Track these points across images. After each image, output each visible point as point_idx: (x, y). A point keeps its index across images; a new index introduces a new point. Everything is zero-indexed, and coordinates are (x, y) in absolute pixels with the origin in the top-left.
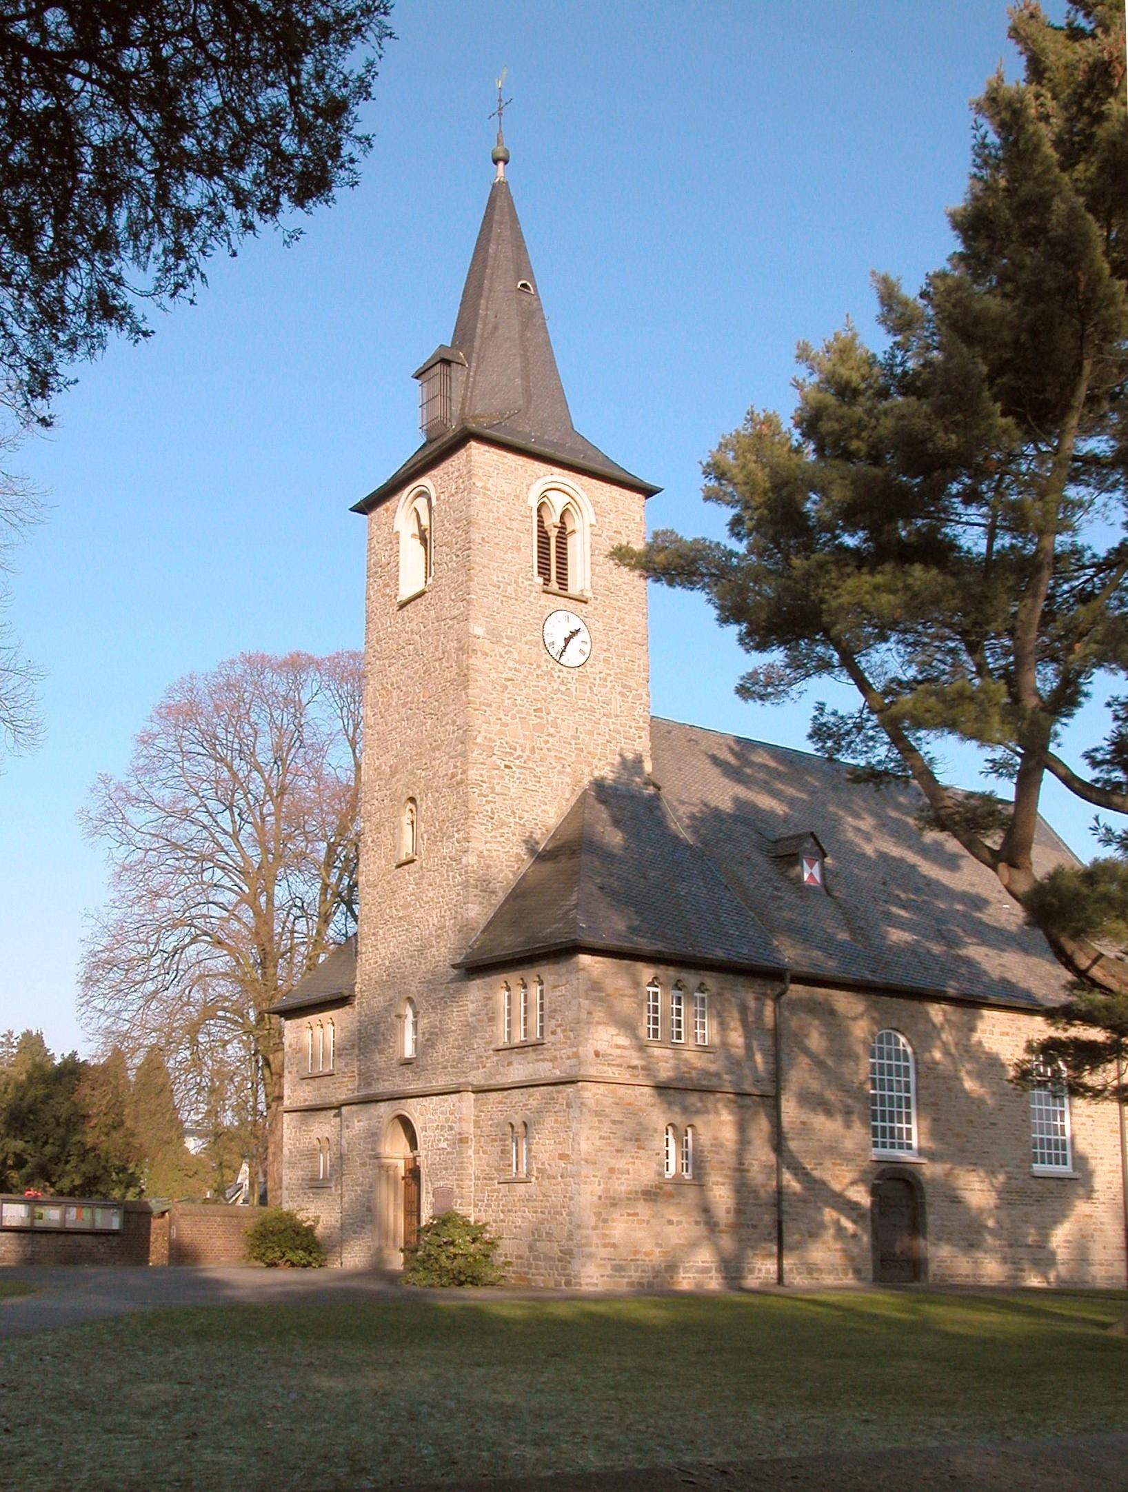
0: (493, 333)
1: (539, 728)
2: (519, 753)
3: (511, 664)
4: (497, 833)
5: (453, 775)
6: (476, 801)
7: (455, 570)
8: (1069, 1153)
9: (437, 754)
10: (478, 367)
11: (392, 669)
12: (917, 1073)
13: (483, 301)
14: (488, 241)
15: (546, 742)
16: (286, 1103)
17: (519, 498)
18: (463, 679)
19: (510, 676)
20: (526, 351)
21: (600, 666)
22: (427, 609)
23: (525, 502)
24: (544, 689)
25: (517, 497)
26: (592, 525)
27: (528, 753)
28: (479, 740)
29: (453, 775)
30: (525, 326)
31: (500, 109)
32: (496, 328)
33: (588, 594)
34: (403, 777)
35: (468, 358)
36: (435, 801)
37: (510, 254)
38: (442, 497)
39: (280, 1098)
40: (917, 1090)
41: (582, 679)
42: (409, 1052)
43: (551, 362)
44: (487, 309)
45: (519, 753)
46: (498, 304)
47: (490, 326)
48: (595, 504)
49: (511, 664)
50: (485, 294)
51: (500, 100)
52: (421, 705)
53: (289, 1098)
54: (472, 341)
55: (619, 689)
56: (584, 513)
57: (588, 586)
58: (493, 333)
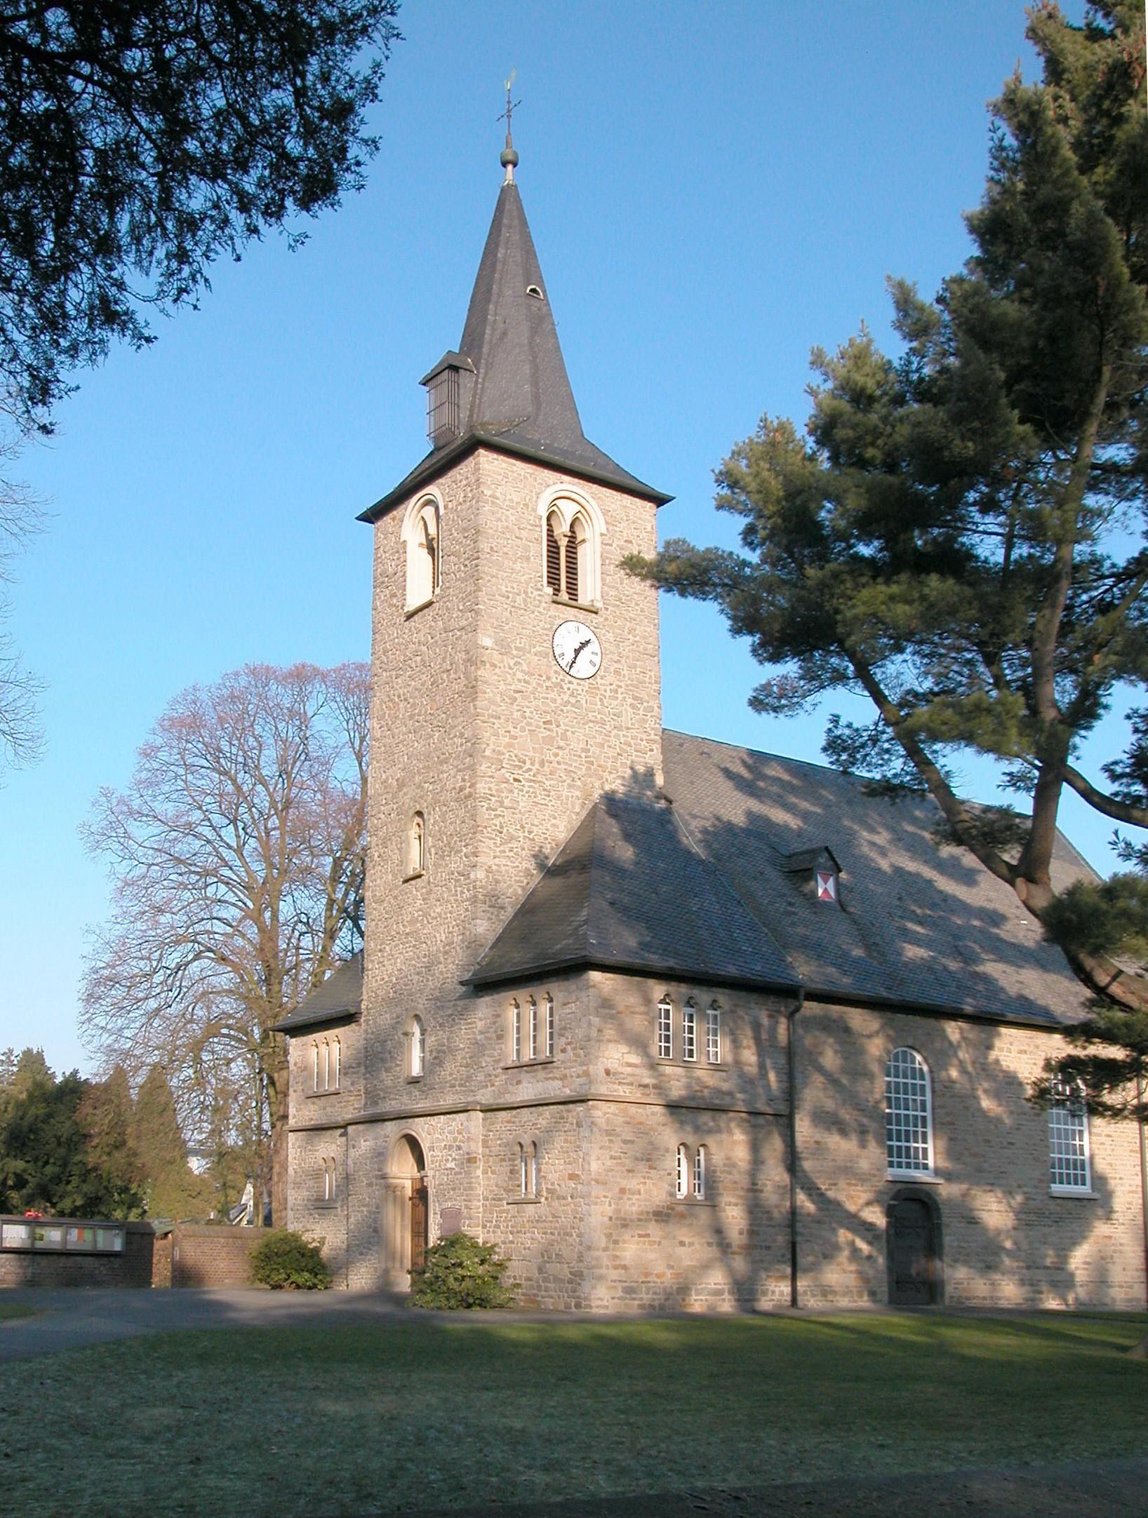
0: (501, 339)
1: (549, 740)
2: (528, 766)
3: (520, 675)
4: (506, 847)
5: (462, 789)
6: (484, 814)
7: (463, 580)
8: (1087, 1173)
9: (445, 767)
10: (486, 374)
11: (399, 680)
12: (933, 1092)
13: (491, 307)
14: (497, 245)
15: (556, 755)
16: (292, 1122)
17: (529, 506)
18: (472, 691)
19: (519, 688)
20: (535, 358)
21: (611, 678)
22: (434, 620)
23: (534, 510)
24: (554, 701)
25: (526, 505)
26: (602, 535)
27: (537, 766)
28: (488, 753)
29: (462, 789)
30: (534, 331)
31: (509, 111)
32: (504, 334)
33: (599, 605)
34: (410, 791)
35: (476, 364)
36: (443, 815)
37: (519, 258)
38: (450, 505)
39: (285, 1117)
40: (933, 1108)
41: (593, 691)
42: (416, 1069)
43: (560, 368)
44: (496, 315)
45: (528, 766)
46: (507, 310)
47: (499, 332)
48: (605, 513)
49: (520, 675)
50: (494, 299)
51: (509, 102)
52: (428, 718)
53: (294, 1117)
54: (480, 347)
55: (630, 701)
56: (595, 521)
57: (599, 597)
58: (501, 339)
